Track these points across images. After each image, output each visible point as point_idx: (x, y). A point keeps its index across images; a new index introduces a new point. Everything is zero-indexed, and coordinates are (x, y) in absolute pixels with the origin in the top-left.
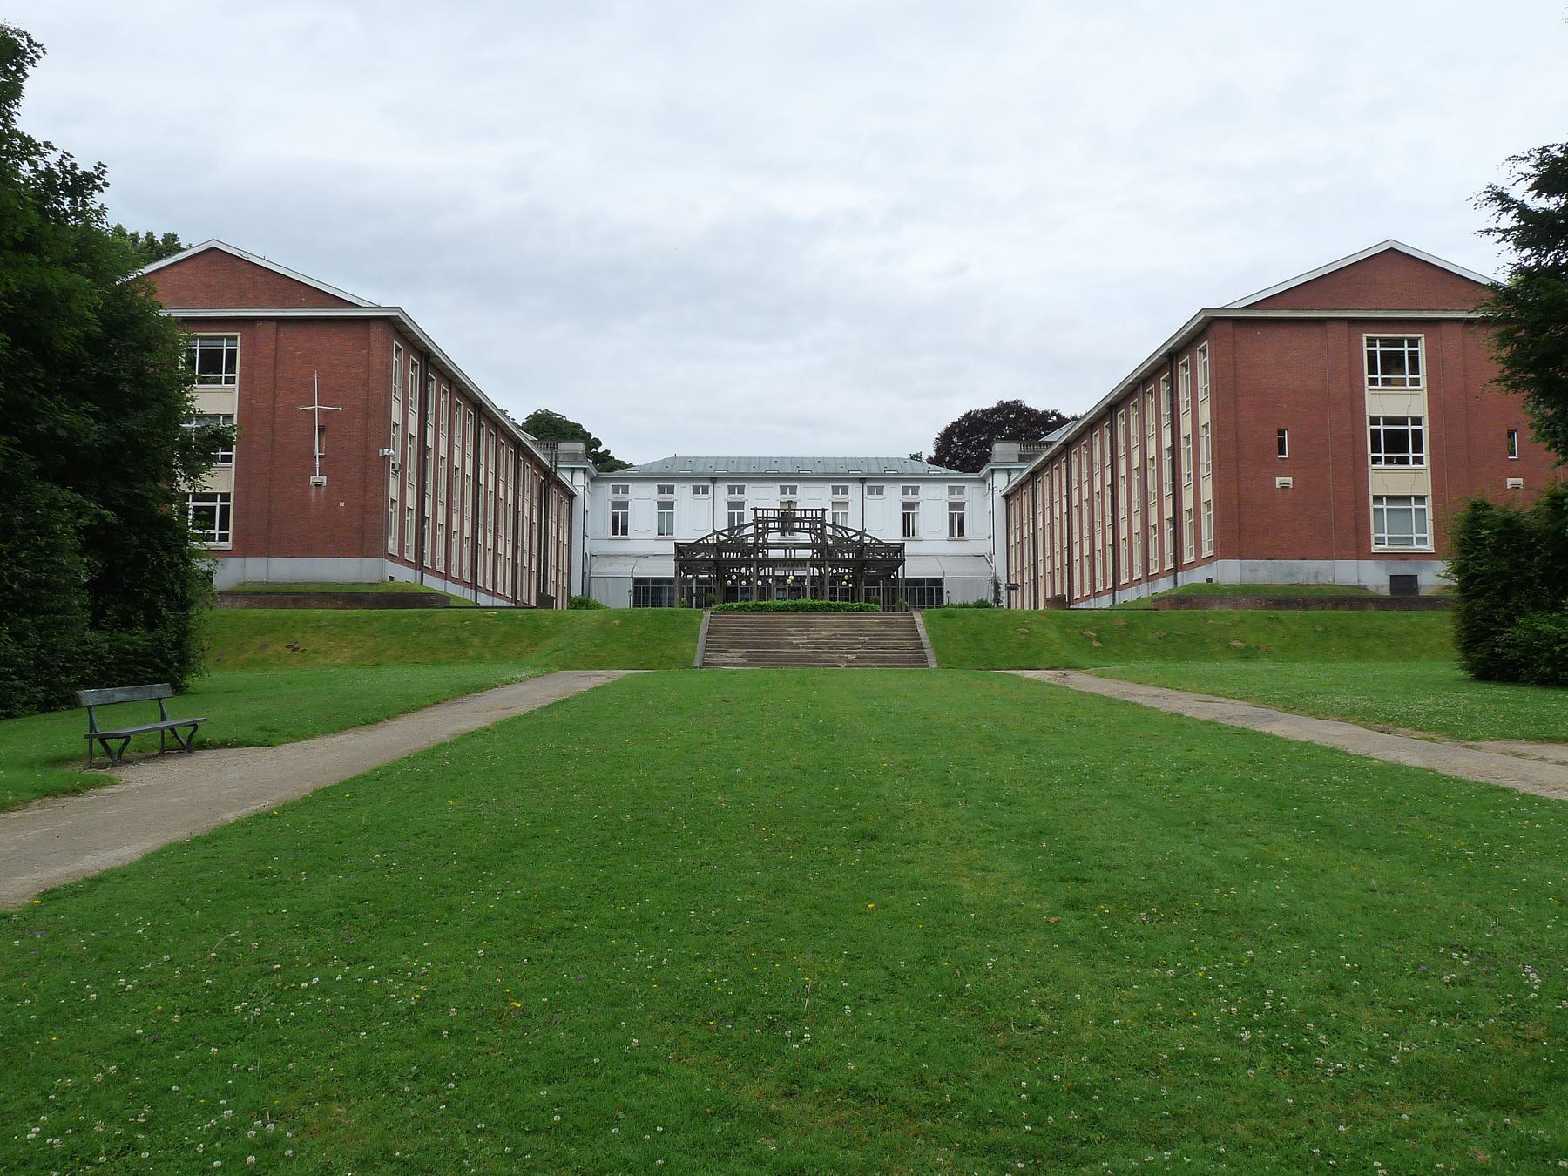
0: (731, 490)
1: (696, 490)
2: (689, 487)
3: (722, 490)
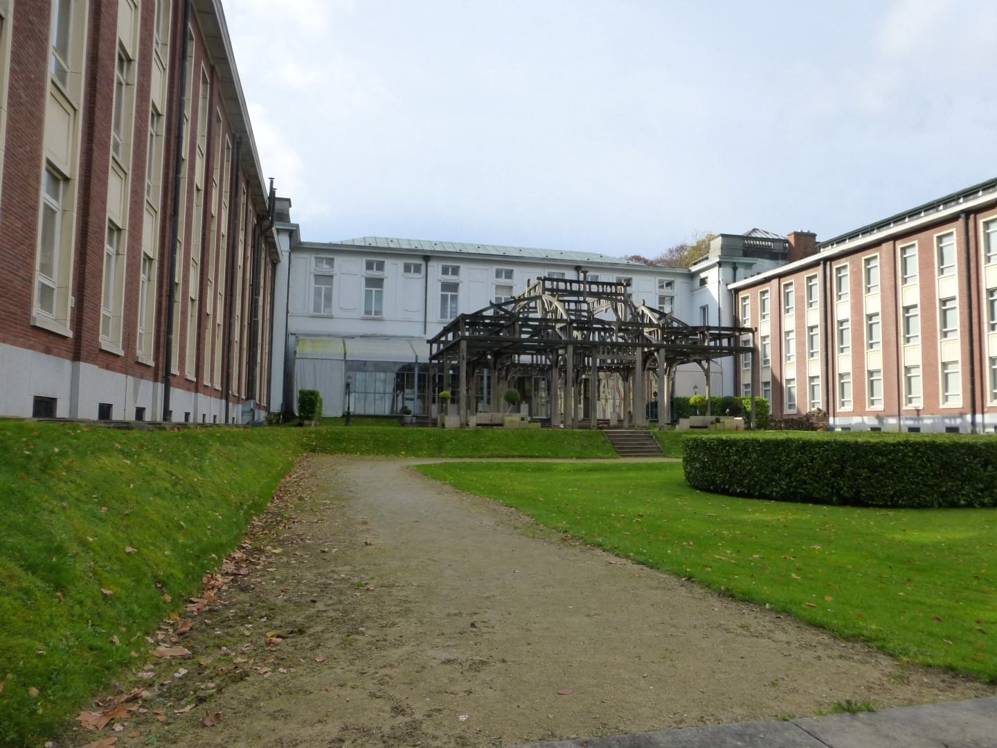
0: (445, 271)
1: (407, 269)
2: (400, 264)
3: (435, 268)
